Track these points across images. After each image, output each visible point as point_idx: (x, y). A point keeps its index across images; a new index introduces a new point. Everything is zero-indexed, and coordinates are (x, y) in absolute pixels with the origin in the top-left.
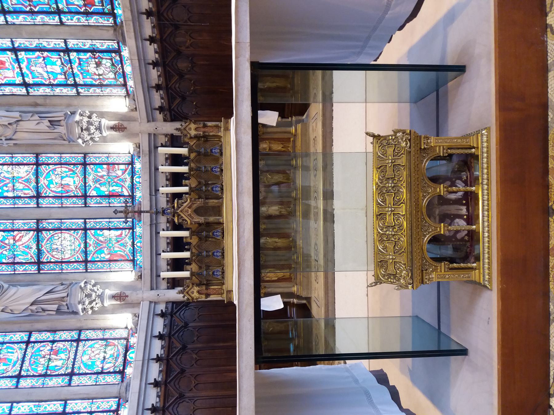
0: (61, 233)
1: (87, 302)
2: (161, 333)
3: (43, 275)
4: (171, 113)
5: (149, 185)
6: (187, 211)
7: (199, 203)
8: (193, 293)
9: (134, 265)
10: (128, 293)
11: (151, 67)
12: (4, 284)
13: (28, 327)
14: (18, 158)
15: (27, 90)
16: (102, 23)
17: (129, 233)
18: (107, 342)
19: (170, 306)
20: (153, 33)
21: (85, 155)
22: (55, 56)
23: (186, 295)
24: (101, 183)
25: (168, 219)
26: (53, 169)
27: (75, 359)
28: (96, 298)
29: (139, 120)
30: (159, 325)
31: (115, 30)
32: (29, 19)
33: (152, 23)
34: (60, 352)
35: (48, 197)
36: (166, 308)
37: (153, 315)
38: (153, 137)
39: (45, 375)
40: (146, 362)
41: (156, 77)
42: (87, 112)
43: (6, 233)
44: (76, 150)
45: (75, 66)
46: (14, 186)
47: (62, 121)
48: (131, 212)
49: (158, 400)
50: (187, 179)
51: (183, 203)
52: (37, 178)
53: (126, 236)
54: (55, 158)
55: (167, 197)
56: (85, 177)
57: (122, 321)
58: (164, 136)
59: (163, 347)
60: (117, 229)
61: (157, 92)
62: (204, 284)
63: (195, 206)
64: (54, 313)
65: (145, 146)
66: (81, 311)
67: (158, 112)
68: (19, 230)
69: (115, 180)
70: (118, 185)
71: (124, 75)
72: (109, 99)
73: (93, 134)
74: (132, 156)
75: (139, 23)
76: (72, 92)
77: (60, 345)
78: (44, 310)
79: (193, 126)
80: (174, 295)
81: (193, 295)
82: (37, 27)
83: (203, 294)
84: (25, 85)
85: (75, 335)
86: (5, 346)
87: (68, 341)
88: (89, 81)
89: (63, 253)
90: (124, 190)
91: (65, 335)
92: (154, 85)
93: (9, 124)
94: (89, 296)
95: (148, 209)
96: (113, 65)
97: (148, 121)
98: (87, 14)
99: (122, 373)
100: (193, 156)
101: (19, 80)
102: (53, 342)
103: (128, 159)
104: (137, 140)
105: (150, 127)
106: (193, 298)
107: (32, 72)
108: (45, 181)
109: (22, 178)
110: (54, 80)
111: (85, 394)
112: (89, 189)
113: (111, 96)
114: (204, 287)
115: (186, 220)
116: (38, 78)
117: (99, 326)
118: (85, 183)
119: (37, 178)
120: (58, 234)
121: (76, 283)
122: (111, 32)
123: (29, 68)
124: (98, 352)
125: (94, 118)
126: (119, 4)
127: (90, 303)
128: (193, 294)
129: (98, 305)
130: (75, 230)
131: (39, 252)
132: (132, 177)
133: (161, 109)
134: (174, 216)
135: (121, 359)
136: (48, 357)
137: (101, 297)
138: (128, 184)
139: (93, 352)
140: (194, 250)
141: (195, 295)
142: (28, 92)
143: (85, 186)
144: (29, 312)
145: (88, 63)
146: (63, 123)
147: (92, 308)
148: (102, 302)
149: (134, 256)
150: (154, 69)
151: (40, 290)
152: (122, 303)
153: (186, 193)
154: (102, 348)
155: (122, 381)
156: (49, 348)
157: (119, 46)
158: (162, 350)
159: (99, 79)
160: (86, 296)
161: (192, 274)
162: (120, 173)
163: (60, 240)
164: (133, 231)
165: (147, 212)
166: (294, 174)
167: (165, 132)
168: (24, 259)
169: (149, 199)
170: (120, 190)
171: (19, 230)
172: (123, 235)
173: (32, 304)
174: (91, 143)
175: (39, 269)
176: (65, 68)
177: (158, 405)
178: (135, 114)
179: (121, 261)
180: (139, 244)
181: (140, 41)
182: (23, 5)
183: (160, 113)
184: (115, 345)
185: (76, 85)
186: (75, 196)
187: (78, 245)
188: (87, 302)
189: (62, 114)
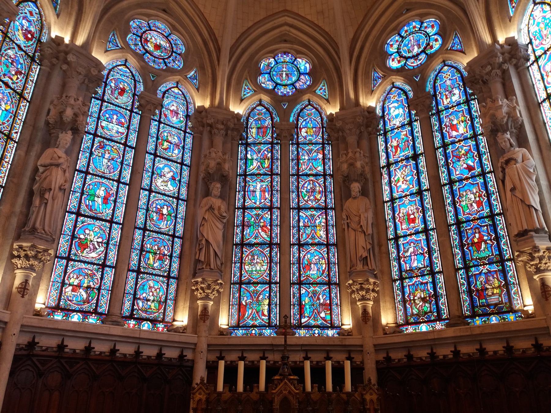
0: (267, 263)
1: (203, 286)
2: (164, 356)
3: (231, 248)
4: (385, 368)
5: (312, 343)
6: (285, 390)
8: (200, 394)
9: (234, 327)
10: (208, 322)
11: (429, 351)
12: (226, 219)
13: (188, 236)
14: (332, 231)
15: (392, 239)
16: (464, 305)
17: (265, 322)
18: (163, 302)
19: (189, 364)
20: (464, 354)
21: (338, 285)
22: (427, 262)
23: (199, 387)
24: (312, 298)
25: (278, 362)
26: (324, 257)
27: (152, 274)
28: (206, 293)
29: (376, 336)
30: (171, 353)
31: (459, 317)
33: (473, 353)
34: (161, 262)
35: (299, 253)
36: (188, 360)
37: (183, 347)
38: (360, 349)
39: (142, 250)
40: (138, 341)
41: (420, 356)
42: (378, 289)
43: (269, 220)
44: (342, 277)
45: (420, 279)
46: (309, 227)
47: (367, 267)
48: (285, 328)
49: (97, 353)
50: (320, 390)
51: (294, 385)
52: (316, 244)
53: (263, 320)
54: (334, 259)
55: (300, 362)
56: (317, 284)
57: (182, 319)
58: (361, 360)
59: (149, 357)
60: (270, 311)
61: (405, 356)
62: (207, 406)
63: (290, 398)
64: (197, 258)
65: (349, 341)
66: (196, 280)
67: (385, 355)
68: (271, 229)
69: (316, 311)
70: (311, 314)
71: (418, 323)
72: (392, 308)
73: (358, 293)
74: (340, 327)
75: (470, 341)
76: (395, 274)
77: (167, 262)
78: (200, 250)
79: (375, 397)
80: (200, 372)
81: (197, 394)
82: (449, 249)
83: (197, 405)
84: (397, 238)
85: (175, 273)
86: (173, 219)
87: (170, 268)
88: (407, 290)
89: (250, 264)
90: (306, 319)
91: (175, 266)
92: (412, 353)
93: (361, 226)
94: (209, 287)
95: (289, 342)
96: (426, 313)
97: (375, 346)
98: (470, 292)
100: (344, 396)
101: (395, 195)
102: (171, 256)
103: (336, 323)
104: (355, 333)
105: (369, 346)
106: (194, 394)
107: (409, 243)
108: (313, 251)
109: (316, 233)
110: (404, 261)
111: (118, 283)
112: (307, 287)
113: (396, 309)
114: (204, 406)
115: (276, 388)
116: (404, 248)
117: (179, 294)
118: (312, 284)
119: (316, 244)
121: (221, 276)
122: (457, 313)
124: (155, 294)
125: (372, 295)
126: (485, 321)
127: (202, 288)
128: (199, 394)
129: (199, 294)
130: (270, 274)
131: (251, 245)
132: (318, 327)
134: (281, 375)
135: (144, 315)
136: (158, 252)
137: (207, 298)
138: (312, 322)
139: (156, 290)
140: (244, 395)
141: (198, 397)
142: (390, 240)
143: (309, 284)
144: (200, 238)
145: (424, 290)
146: (366, 268)
147: (197, 289)
148: (201, 299)
149: (243, 327)
150: (428, 353)
151: (218, 247)
152: (199, 317)
153: (304, 388)
154: (158, 298)
155: (123, 317)
156: (166, 252)
157: (445, 320)
158: (146, 357)
159: (410, 300)
160: (209, 284)
161: (220, 394)
162: (323, 315)
163: (262, 261)
164: (266, 327)
165: (285, 341)
166: (519, 350)
167: (365, 361)
168: (247, 234)
169: (298, 343)
170: (306, 315)
171: (271, 229)
172: (263, 317)
173: (207, 241)
174: (349, 291)
175: (237, 245)
176: (416, 271)
177: (92, 353)
178: (380, 333)
179: (239, 315)
180: (253, 332)
181: (453, 341)
182: (468, 238)
183: (384, 358)
184: (159, 310)
186: (300, 275)
187: (256, 277)
188: (203, 286)
189: (374, 267)
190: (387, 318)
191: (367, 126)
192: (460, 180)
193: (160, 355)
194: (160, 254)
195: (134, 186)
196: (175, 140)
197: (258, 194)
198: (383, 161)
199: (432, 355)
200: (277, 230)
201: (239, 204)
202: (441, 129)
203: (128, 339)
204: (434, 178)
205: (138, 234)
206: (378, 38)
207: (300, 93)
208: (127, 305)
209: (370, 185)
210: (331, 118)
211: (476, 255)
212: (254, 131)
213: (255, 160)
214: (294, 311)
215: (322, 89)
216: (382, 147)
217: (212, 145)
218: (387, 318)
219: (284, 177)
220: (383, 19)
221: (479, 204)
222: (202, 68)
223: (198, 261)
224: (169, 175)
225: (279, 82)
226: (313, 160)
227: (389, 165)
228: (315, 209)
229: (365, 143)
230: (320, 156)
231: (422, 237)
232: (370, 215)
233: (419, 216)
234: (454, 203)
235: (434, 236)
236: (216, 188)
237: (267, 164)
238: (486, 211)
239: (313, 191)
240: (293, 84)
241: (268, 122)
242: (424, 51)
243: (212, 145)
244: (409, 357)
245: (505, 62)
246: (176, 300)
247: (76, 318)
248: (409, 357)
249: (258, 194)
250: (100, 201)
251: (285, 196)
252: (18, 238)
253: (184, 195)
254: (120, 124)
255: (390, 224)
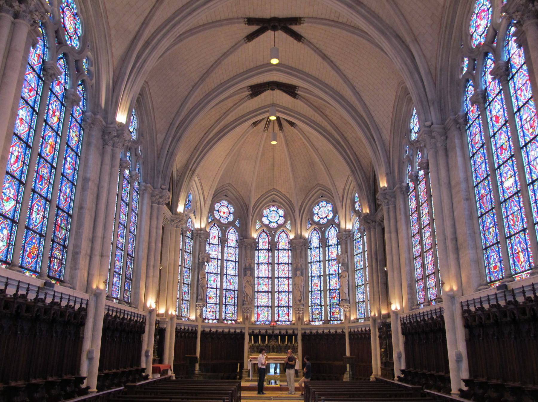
7: (275, 346)
14: (291, 286)
32: (328, 296)
37: (241, 329)
38: (297, 329)
54: (291, 297)
76: (310, 304)
84: (312, 291)
91: (236, 301)
98: (330, 313)
99: (225, 319)
105: (299, 328)
120: (267, 297)
123: (316, 293)
125: (302, 312)
133: (305, 332)
137: (248, 313)
138: (282, 320)
173: (247, 294)
185: (312, 306)
187: (263, 304)
190: (306, 319)
191: (305, 245)
192: (332, 275)
193: (235, 331)
194: (232, 299)
195: (222, 274)
196: (232, 252)
197: (263, 271)
198: (309, 261)
199: (317, 332)
200: (270, 286)
201: (256, 275)
202: (328, 253)
203: (226, 327)
204: (325, 272)
205: (224, 292)
206: (311, 205)
207: (280, 226)
208: (223, 316)
209: (304, 271)
210: (291, 240)
211: (333, 301)
212: (261, 243)
213: (262, 256)
214: (276, 316)
215: (288, 226)
216: (309, 254)
217: (246, 257)
218: (306, 319)
219: (272, 264)
220: (313, 198)
221: (336, 284)
222: (240, 218)
223: (244, 300)
224: (232, 267)
225: (271, 220)
226: (284, 257)
227: (311, 262)
228: (285, 278)
229: (303, 253)
230: (287, 255)
231: (319, 292)
232: (303, 283)
233: (319, 284)
234: (329, 282)
235: (323, 292)
236: (249, 273)
237: (267, 258)
238: (338, 287)
239: (284, 270)
240: (276, 222)
241: (267, 240)
242: (326, 217)
243: (246, 257)
244: (311, 332)
245: (346, 238)
246: (237, 313)
247: (211, 321)
248: (311, 332)
249: (263, 271)
250: (212, 282)
251: (273, 271)
252: (197, 302)
253: (237, 274)
254: (215, 251)
255: (310, 285)
